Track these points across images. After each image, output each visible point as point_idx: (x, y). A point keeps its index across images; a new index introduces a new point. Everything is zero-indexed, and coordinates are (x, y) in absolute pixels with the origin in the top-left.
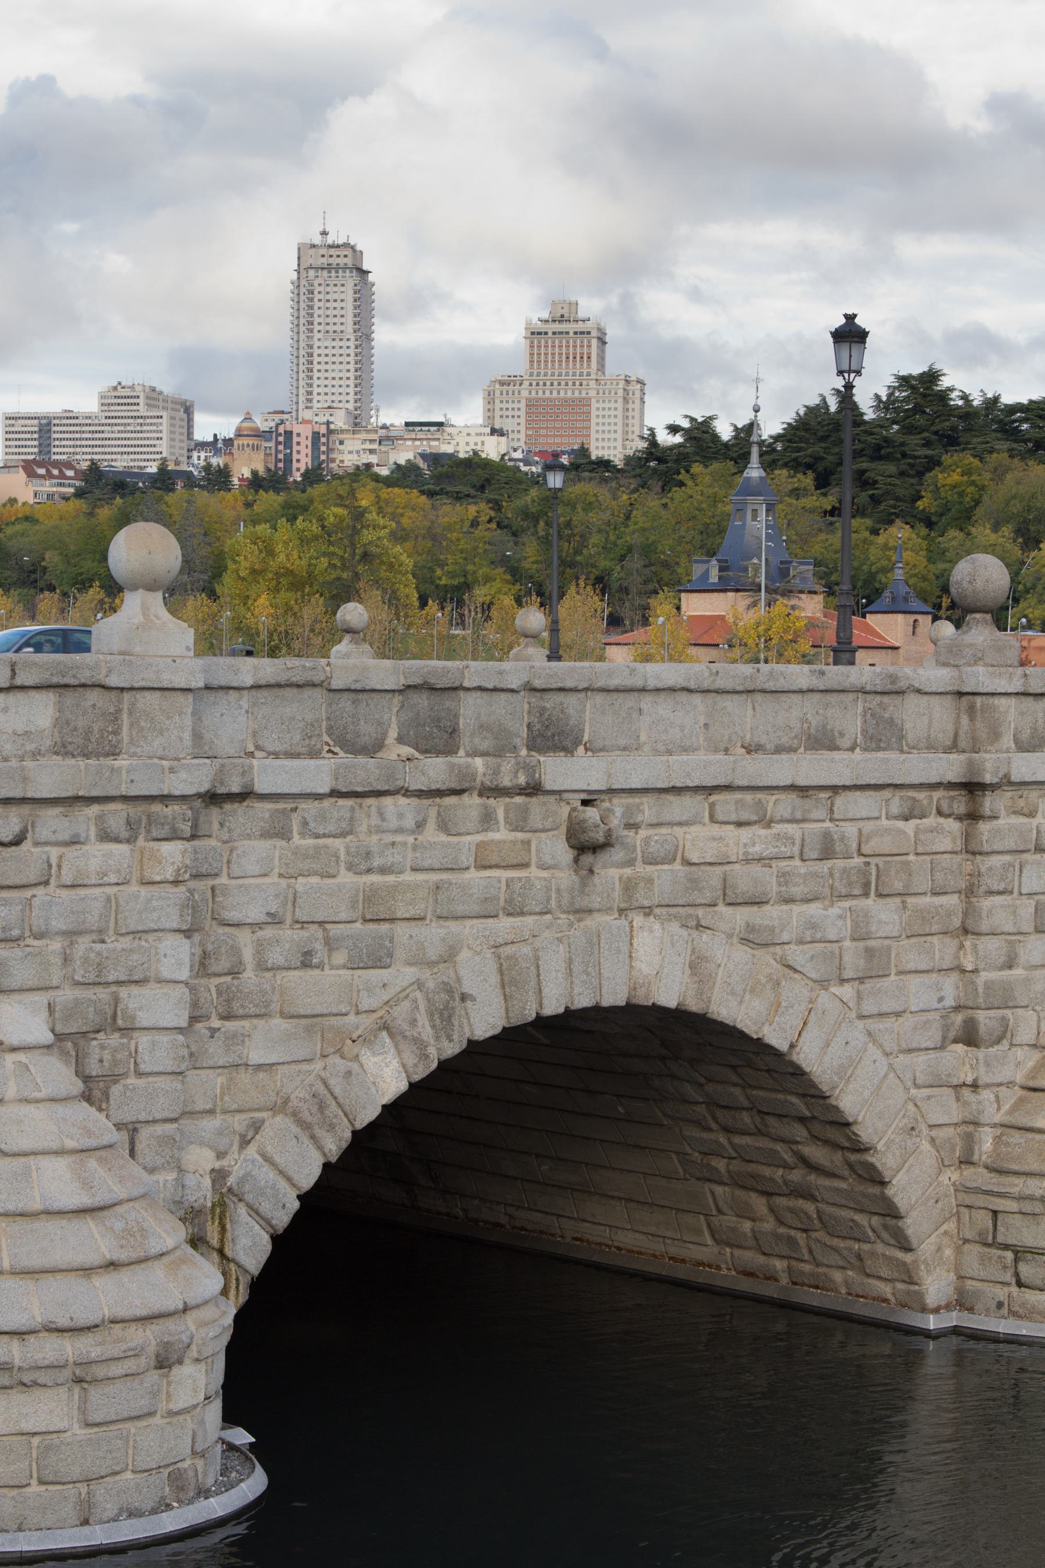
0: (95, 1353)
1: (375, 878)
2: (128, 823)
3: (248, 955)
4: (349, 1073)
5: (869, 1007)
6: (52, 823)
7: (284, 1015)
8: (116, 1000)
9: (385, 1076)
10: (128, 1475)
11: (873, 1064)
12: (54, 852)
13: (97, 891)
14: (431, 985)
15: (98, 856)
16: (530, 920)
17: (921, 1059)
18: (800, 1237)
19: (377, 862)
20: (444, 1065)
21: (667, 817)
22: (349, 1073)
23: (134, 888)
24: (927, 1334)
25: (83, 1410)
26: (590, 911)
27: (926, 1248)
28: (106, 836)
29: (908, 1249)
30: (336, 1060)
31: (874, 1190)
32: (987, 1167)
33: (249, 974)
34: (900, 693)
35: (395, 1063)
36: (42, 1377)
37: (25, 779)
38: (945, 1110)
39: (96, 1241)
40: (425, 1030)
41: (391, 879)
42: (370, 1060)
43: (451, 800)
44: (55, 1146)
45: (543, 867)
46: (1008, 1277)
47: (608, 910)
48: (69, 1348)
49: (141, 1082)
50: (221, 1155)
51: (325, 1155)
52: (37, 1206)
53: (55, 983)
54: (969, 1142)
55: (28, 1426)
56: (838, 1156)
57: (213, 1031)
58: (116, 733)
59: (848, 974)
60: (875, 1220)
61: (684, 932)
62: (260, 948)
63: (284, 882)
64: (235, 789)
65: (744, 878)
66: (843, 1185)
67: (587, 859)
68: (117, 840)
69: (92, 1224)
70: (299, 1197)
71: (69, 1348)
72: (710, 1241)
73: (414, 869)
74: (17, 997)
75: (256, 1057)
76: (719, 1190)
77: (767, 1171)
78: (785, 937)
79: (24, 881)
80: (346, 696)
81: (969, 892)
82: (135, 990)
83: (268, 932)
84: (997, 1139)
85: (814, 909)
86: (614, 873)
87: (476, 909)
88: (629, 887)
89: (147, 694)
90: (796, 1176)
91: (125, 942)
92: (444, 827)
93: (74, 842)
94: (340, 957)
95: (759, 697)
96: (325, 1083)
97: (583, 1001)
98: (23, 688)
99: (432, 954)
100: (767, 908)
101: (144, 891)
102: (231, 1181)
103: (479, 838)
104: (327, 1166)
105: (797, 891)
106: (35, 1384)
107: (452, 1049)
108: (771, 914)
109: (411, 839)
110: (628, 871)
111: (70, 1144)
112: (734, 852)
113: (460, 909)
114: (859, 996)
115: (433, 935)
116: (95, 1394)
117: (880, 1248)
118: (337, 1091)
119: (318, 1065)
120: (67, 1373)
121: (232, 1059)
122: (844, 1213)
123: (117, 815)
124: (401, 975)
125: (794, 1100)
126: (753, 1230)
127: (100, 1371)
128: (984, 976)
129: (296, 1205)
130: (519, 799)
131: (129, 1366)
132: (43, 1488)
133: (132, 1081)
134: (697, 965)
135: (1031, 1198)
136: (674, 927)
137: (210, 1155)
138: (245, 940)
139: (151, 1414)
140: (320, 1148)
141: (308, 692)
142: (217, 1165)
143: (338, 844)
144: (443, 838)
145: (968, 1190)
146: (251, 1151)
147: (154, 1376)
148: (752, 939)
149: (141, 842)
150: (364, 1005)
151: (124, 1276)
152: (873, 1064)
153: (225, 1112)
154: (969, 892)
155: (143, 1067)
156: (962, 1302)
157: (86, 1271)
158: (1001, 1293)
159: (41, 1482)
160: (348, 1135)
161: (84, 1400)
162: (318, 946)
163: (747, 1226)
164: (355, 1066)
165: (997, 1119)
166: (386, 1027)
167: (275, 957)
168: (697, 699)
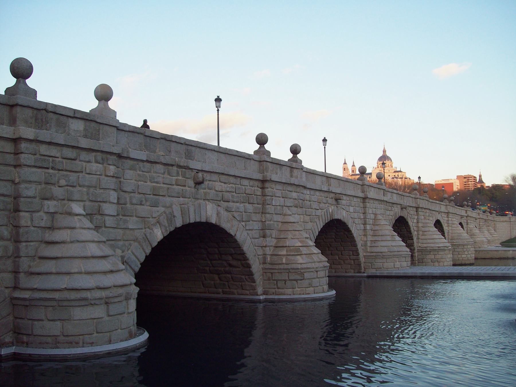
0: (111, 295)
1: (154, 184)
2: (102, 159)
3: (128, 200)
4: (151, 233)
5: (247, 228)
6: (84, 155)
7: (137, 217)
8: (100, 206)
9: (158, 235)
10: (119, 330)
11: (249, 241)
12: (84, 164)
13: (95, 176)
14: (167, 212)
15: (95, 167)
16: (186, 199)
17: (256, 240)
18: (226, 283)
19: (156, 180)
20: (171, 232)
21: (212, 179)
22: (151, 233)
23: (103, 177)
24: (260, 301)
25: (108, 311)
26: (198, 199)
27: (258, 282)
28: (97, 162)
29: (255, 282)
30: (147, 229)
31: (248, 269)
32: (269, 264)
33: (128, 205)
34: (250, 159)
35: (160, 231)
36: (97, 302)
37: (78, 142)
38: (260, 252)
39: (104, 265)
40: (166, 223)
41: (159, 185)
42: (155, 230)
43: (170, 167)
44: (92, 239)
45: (189, 187)
46: (276, 287)
47: (201, 199)
48: (103, 294)
49: (106, 229)
50: (123, 252)
51: (146, 253)
52: (89, 255)
53: (85, 199)
54: (265, 258)
55: (93, 317)
56: (239, 263)
57: (121, 219)
58: (99, 135)
59: (244, 220)
60: (247, 277)
61: (216, 206)
62: (131, 198)
63: (136, 182)
64: (125, 156)
65: (227, 196)
66: (240, 269)
67: (197, 186)
68: (100, 163)
69: (104, 261)
70: (141, 264)
71: (103, 294)
72: (202, 287)
73: (164, 184)
74: (75, 202)
75: (130, 227)
76: (206, 275)
77: (220, 269)
78: (233, 210)
79: (77, 170)
80: (148, 138)
81: (263, 204)
82: (104, 204)
83: (132, 194)
84: (271, 258)
85: (238, 204)
86: (202, 190)
87: (176, 195)
88: (205, 194)
89: (106, 126)
90: (227, 269)
91: (102, 191)
92: (169, 174)
93: (89, 162)
94: (148, 204)
95: (227, 155)
96: (146, 236)
97: (198, 220)
98: (77, 118)
99: (168, 205)
100: (230, 203)
101: (106, 178)
102: (125, 259)
103: (176, 178)
104: (146, 256)
105: (235, 200)
106: (95, 304)
107: (172, 229)
108: (231, 204)
109: (162, 176)
110: (205, 191)
111: (96, 239)
112: (224, 190)
113: (173, 195)
114: (246, 225)
115: (168, 199)
116: (111, 307)
117: (247, 283)
118: (148, 237)
119: (144, 230)
120: (103, 301)
121: (125, 227)
122: (238, 276)
123: (99, 156)
124: (161, 209)
125: (231, 249)
126: (214, 283)
127: (113, 300)
128: (267, 222)
129: (140, 266)
130: (184, 170)
131: (119, 299)
132: (98, 334)
133: (103, 229)
134: (218, 214)
135: (280, 269)
136: (214, 205)
137: (120, 251)
138: (127, 195)
139: (124, 313)
140: (145, 252)
141: (140, 135)
142: (122, 254)
143: (147, 174)
144: (169, 177)
145: (266, 269)
146: (130, 251)
147: (124, 302)
148: (228, 210)
149: (105, 165)
150: (154, 216)
151: (115, 275)
152: (249, 241)
153: (124, 240)
154: (263, 204)
155: (107, 225)
156: (265, 293)
157: (105, 273)
158: (274, 290)
159: (97, 333)
160: (151, 249)
161: (108, 309)
162: (144, 199)
163: (213, 282)
164: (152, 231)
165: (270, 253)
166: (158, 222)
167: (134, 201)
168: (216, 153)
